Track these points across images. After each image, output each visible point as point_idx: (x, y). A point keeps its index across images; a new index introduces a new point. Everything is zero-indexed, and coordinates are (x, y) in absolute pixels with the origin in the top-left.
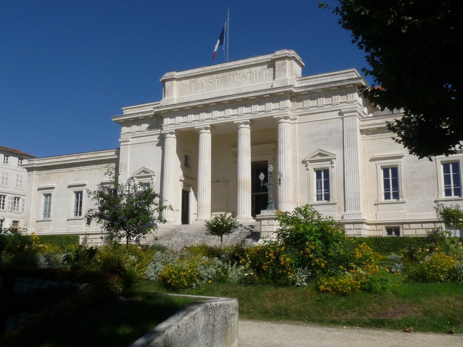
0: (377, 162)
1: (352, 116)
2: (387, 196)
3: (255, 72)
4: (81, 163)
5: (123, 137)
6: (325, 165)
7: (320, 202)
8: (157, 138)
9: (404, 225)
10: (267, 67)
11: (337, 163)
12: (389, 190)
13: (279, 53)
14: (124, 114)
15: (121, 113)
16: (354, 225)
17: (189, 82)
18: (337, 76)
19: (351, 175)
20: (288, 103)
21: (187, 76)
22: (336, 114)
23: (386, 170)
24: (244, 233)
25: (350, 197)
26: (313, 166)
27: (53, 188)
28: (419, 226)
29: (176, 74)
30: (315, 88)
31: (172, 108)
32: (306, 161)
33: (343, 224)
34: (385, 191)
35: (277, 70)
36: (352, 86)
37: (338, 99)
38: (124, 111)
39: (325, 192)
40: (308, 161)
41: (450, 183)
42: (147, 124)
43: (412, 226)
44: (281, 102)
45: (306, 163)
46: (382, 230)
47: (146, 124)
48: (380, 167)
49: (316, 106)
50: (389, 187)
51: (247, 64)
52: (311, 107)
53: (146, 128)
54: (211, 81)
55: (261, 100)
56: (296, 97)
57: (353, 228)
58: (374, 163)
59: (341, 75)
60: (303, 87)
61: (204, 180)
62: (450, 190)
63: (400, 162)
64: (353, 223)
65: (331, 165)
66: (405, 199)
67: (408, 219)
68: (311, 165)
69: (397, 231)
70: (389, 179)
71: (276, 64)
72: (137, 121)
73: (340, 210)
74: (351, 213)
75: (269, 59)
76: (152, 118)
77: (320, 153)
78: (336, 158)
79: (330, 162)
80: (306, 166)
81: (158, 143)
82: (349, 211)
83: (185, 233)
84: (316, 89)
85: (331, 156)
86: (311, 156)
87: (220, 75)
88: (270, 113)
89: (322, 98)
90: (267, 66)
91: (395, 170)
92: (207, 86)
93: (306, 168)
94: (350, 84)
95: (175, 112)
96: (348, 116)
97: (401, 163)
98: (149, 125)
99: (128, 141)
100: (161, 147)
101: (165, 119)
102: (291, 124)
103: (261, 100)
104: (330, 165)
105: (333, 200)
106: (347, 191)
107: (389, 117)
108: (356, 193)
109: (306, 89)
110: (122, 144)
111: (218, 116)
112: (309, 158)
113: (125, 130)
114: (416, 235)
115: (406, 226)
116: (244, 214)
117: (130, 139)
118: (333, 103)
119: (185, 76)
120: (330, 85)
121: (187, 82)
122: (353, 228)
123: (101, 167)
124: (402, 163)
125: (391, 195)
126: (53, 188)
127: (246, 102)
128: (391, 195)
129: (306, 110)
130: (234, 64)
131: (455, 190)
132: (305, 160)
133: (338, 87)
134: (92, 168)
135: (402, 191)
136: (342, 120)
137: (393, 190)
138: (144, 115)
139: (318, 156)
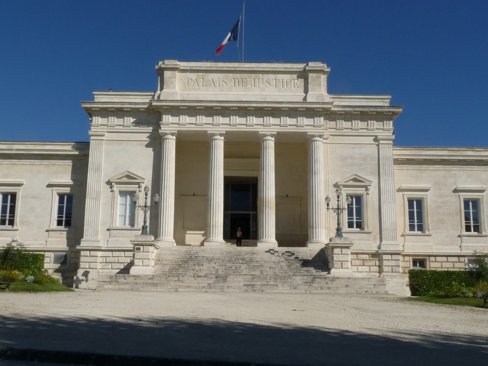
0: (405, 193)
1: (97, 140)
2: (412, 228)
3: (219, 79)
4: (431, 160)
5: (93, 130)
6: (359, 191)
7: (351, 230)
8: (147, 138)
9: (431, 257)
10: (296, 77)
11: (373, 190)
12: (414, 222)
13: (312, 65)
14: (96, 100)
15: (91, 98)
16: (393, 255)
17: (196, 77)
18: (372, 100)
19: (388, 204)
20: (321, 120)
21: (194, 68)
22: (370, 140)
23: (411, 202)
24: (291, 261)
25: (387, 227)
26: (346, 191)
27: (20, 185)
28: (445, 259)
29: (183, 65)
30: (354, 110)
31: (179, 104)
32: (112, 182)
33: (380, 254)
34: (410, 222)
35: (311, 83)
36: (391, 113)
37: (376, 124)
38: (95, 96)
39: (357, 219)
40: (114, 182)
41: (6, 213)
42: (133, 118)
43: (438, 259)
44: (181, 116)
45: (112, 184)
46: (410, 262)
47: (131, 118)
48: (56, 194)
49: (107, 125)
50: (414, 219)
51: (273, 70)
52: (345, 129)
53: (132, 123)
54: (225, 80)
55: (293, 112)
56: (329, 115)
57: (89, 255)
58: (401, 193)
59: (376, 100)
60: (341, 106)
61: (219, 195)
62: (5, 220)
63: (427, 195)
64: (392, 254)
65: (138, 189)
66: (431, 232)
67: (435, 251)
68: (116, 187)
69: (422, 263)
70: (64, 206)
71: (309, 76)
72: (120, 112)
73: (375, 239)
74: (394, 244)
75: (300, 68)
76: (142, 111)
77: (355, 178)
78: (144, 182)
79: (137, 186)
80: (111, 187)
81: (149, 143)
82: (385, 241)
83: (211, 257)
84: (355, 111)
85: (367, 182)
86: (117, 178)
87: (238, 76)
88: (303, 128)
89: (129, 118)
90: (297, 76)
91: (420, 202)
92: (221, 85)
93: (111, 190)
94: (390, 112)
95: (183, 109)
96: (95, 140)
97: (427, 196)
98: (135, 119)
99: (103, 136)
100: (152, 149)
101: (164, 116)
102: (323, 143)
103: (293, 112)
104: (364, 191)
105: (368, 229)
106: (384, 221)
107: (39, 144)
108: (393, 224)
109: (344, 109)
110: (92, 138)
111: (239, 124)
112: (343, 182)
113: (97, 120)
114: (442, 267)
115: (432, 259)
116: (168, 237)
117: (106, 134)
118: (109, 124)
119: (191, 68)
120: (370, 109)
121: (193, 76)
122: (89, 255)
123: (48, 163)
124: (428, 196)
125: (416, 227)
126: (20, 185)
127: (275, 112)
128: (416, 227)
129: (339, 131)
130: (239, 66)
131: (474, 226)
132: (111, 181)
133: (377, 112)
134: (32, 163)
135: (428, 224)
136: (377, 147)
137: (417, 222)
138: (133, 106)
139: (351, 182)
